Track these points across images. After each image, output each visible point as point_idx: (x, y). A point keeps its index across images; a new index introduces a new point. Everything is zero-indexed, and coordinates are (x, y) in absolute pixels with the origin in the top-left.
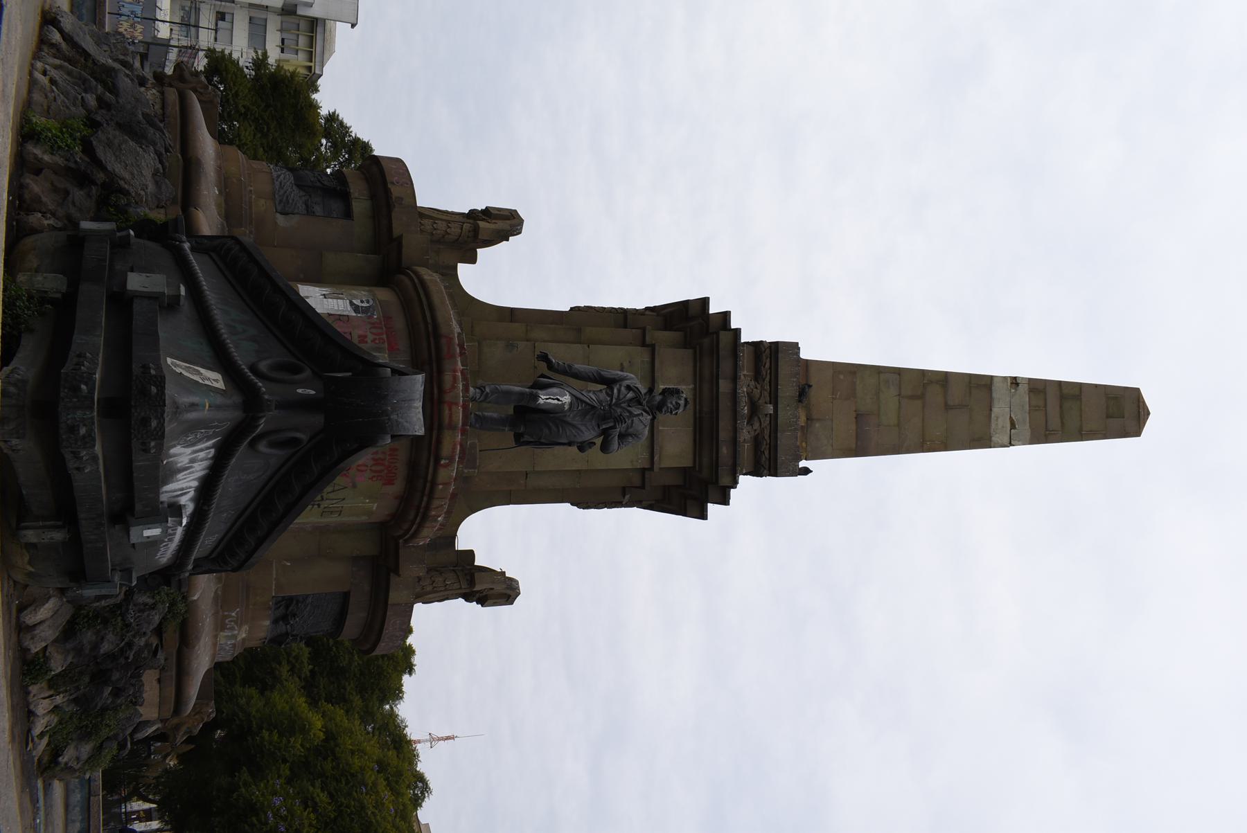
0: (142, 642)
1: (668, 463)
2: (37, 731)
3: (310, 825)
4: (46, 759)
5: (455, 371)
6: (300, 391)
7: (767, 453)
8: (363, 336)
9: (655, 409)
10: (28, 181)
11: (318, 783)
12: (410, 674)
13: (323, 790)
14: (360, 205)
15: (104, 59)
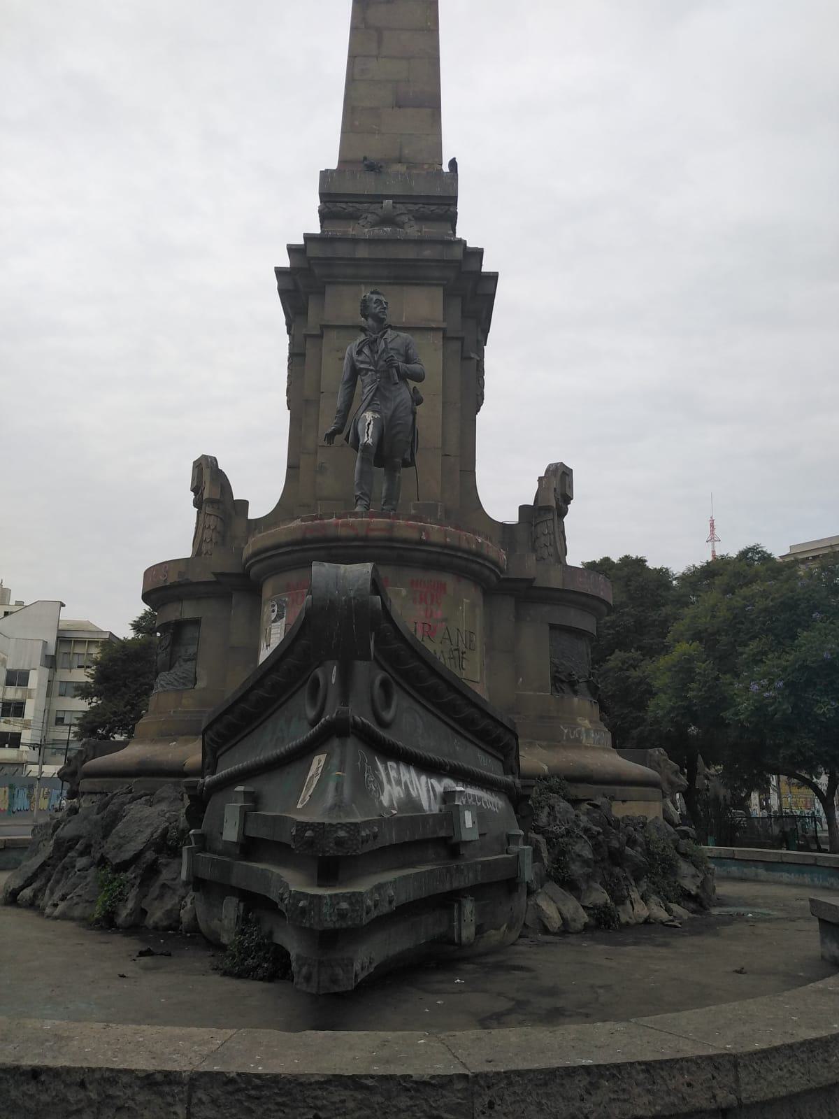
0: (584, 818)
1: (439, 314)
2: (663, 915)
3: (779, 658)
4: (692, 906)
5: (337, 525)
6: (333, 681)
7: (433, 208)
8: (296, 612)
9: (382, 325)
10: (151, 922)
11: (740, 649)
12: (646, 561)
13: (746, 645)
14: (187, 611)
15: (48, 848)
